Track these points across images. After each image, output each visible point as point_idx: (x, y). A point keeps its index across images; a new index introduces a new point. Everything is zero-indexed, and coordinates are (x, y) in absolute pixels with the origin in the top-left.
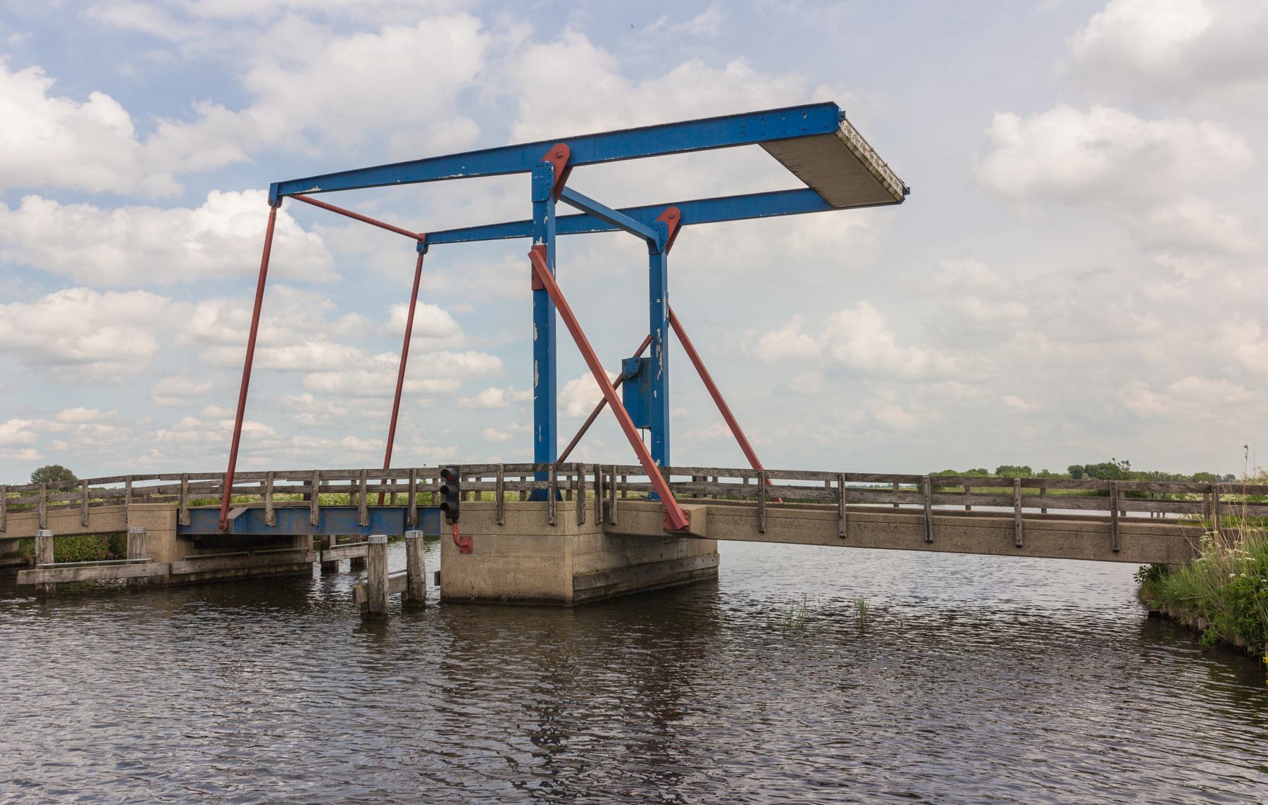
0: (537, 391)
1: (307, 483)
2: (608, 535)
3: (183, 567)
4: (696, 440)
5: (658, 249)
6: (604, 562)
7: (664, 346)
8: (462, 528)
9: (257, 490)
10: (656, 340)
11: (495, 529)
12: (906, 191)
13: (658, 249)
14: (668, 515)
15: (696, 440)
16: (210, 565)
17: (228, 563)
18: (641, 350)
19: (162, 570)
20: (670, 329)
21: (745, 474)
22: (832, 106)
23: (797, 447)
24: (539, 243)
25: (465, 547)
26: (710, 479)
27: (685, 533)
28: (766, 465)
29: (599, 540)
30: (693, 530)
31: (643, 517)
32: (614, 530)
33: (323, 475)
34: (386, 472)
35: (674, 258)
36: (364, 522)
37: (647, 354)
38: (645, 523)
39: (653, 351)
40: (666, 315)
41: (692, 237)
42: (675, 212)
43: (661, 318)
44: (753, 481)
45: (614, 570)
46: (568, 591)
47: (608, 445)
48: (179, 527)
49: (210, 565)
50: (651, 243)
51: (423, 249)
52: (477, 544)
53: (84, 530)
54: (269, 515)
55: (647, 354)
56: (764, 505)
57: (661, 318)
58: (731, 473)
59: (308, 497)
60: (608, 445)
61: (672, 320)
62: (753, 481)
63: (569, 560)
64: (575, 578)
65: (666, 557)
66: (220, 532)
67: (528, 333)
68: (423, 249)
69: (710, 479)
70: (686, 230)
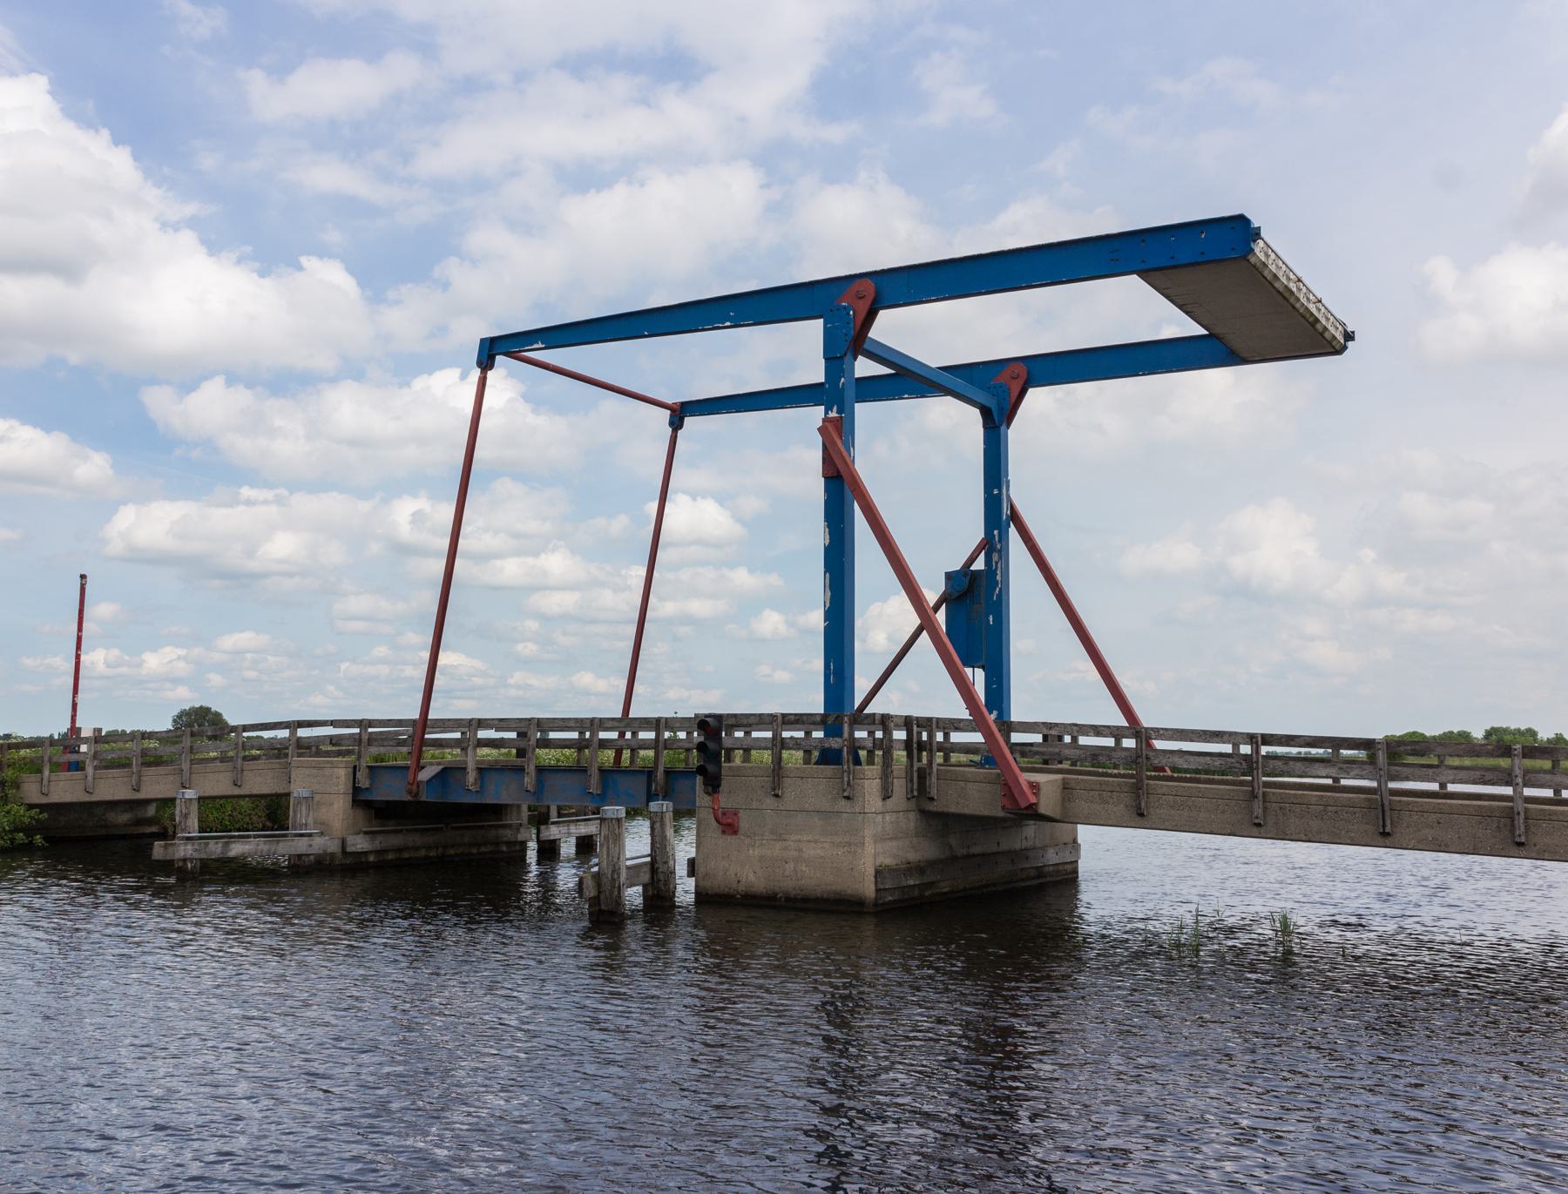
1: (521, 735)
3: (359, 844)
4: (1048, 684)
5: (997, 420)
6: (927, 850)
8: (725, 800)
10: (992, 545)
11: (770, 802)
12: (1349, 336)
14: (1009, 788)
15: (1048, 684)
16: (395, 841)
18: (972, 560)
19: (333, 847)
20: (1013, 530)
21: (1117, 733)
22: (1241, 220)
23: (1193, 695)
24: (833, 414)
25: (729, 826)
26: (1067, 739)
28: (1147, 721)
29: (911, 821)
30: (1042, 810)
32: (932, 807)
34: (625, 722)
35: (1017, 434)
36: (594, 787)
37: (979, 565)
38: (976, 799)
40: (1006, 511)
43: (999, 515)
47: (925, 690)
48: (356, 790)
49: (395, 841)
50: (986, 413)
51: (676, 424)
52: (744, 823)
54: (471, 776)
55: (979, 565)
56: (1147, 778)
57: (999, 515)
58: (1097, 730)
59: (521, 753)
60: (925, 690)
61: (1015, 517)
62: (1129, 743)
63: (870, 849)
64: (878, 873)
65: (1004, 847)
66: (409, 798)
67: (816, 536)
68: (676, 424)
69: (1067, 739)
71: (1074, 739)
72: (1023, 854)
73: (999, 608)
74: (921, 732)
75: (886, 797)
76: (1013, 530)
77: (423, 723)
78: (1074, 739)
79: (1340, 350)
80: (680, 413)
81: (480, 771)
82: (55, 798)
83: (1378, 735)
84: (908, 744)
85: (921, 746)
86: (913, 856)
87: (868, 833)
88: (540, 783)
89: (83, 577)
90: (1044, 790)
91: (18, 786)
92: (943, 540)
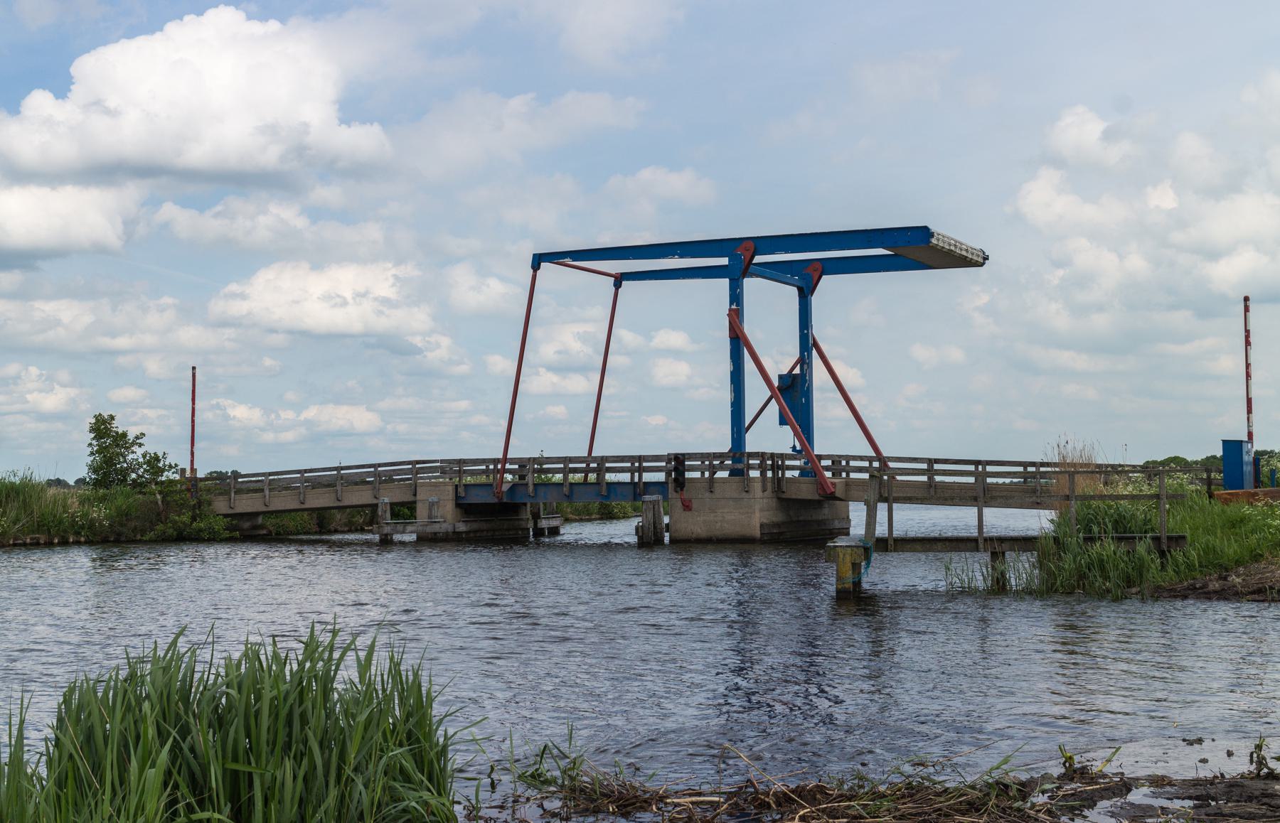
0: (733, 405)
1: (522, 466)
2: (779, 498)
3: (462, 527)
4: (834, 435)
5: (805, 294)
6: (778, 517)
7: (810, 365)
8: (686, 495)
9: (483, 472)
10: (804, 361)
11: (707, 494)
12: (986, 258)
13: (805, 294)
14: (821, 483)
15: (834, 435)
16: (475, 526)
17: (484, 526)
18: (793, 368)
19: (450, 529)
20: (814, 352)
21: (870, 459)
22: (926, 229)
23: (908, 436)
24: (734, 307)
25: (687, 507)
26: (844, 463)
27: (833, 497)
28: (885, 454)
29: (774, 503)
30: (837, 494)
31: (804, 487)
32: (784, 496)
33: (849, 458)
34: (589, 458)
35: (816, 300)
36: (604, 493)
37: (797, 371)
38: (807, 491)
39: (802, 369)
40: (811, 341)
41: (828, 283)
42: (819, 265)
43: (808, 344)
44: (876, 464)
45: (783, 523)
46: (757, 533)
47: (772, 436)
48: (457, 497)
49: (475, 526)
50: (800, 290)
51: (618, 285)
52: (695, 505)
53: (264, 509)
54: (531, 488)
55: (797, 371)
56: (884, 483)
57: (808, 344)
58: (861, 458)
59: (522, 477)
60: (772, 436)
61: (816, 345)
62: (876, 464)
63: (758, 515)
64: (762, 526)
65: (814, 518)
66: (496, 500)
67: (726, 366)
68: (618, 285)
69: (844, 463)
70: (825, 279)
71: (848, 463)
72: (819, 522)
73: (808, 394)
74: (774, 462)
75: (764, 491)
76: (814, 352)
77: (505, 460)
78: (848, 463)
79: (982, 265)
80: (619, 279)
81: (535, 485)
82: (239, 510)
83: (769, 450)
84: (772, 465)
85: (779, 467)
86: (774, 519)
87: (757, 507)
88: (571, 491)
89: (194, 368)
90: (838, 487)
91: (210, 504)
92: (779, 357)
